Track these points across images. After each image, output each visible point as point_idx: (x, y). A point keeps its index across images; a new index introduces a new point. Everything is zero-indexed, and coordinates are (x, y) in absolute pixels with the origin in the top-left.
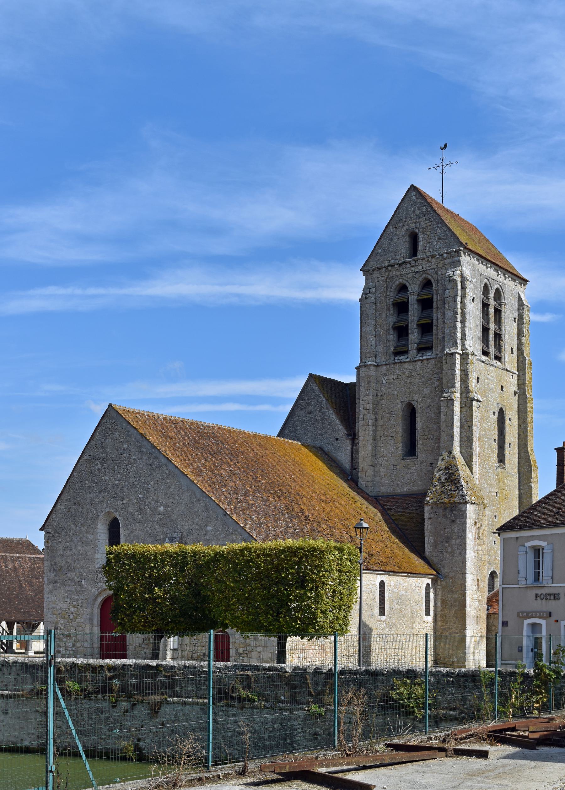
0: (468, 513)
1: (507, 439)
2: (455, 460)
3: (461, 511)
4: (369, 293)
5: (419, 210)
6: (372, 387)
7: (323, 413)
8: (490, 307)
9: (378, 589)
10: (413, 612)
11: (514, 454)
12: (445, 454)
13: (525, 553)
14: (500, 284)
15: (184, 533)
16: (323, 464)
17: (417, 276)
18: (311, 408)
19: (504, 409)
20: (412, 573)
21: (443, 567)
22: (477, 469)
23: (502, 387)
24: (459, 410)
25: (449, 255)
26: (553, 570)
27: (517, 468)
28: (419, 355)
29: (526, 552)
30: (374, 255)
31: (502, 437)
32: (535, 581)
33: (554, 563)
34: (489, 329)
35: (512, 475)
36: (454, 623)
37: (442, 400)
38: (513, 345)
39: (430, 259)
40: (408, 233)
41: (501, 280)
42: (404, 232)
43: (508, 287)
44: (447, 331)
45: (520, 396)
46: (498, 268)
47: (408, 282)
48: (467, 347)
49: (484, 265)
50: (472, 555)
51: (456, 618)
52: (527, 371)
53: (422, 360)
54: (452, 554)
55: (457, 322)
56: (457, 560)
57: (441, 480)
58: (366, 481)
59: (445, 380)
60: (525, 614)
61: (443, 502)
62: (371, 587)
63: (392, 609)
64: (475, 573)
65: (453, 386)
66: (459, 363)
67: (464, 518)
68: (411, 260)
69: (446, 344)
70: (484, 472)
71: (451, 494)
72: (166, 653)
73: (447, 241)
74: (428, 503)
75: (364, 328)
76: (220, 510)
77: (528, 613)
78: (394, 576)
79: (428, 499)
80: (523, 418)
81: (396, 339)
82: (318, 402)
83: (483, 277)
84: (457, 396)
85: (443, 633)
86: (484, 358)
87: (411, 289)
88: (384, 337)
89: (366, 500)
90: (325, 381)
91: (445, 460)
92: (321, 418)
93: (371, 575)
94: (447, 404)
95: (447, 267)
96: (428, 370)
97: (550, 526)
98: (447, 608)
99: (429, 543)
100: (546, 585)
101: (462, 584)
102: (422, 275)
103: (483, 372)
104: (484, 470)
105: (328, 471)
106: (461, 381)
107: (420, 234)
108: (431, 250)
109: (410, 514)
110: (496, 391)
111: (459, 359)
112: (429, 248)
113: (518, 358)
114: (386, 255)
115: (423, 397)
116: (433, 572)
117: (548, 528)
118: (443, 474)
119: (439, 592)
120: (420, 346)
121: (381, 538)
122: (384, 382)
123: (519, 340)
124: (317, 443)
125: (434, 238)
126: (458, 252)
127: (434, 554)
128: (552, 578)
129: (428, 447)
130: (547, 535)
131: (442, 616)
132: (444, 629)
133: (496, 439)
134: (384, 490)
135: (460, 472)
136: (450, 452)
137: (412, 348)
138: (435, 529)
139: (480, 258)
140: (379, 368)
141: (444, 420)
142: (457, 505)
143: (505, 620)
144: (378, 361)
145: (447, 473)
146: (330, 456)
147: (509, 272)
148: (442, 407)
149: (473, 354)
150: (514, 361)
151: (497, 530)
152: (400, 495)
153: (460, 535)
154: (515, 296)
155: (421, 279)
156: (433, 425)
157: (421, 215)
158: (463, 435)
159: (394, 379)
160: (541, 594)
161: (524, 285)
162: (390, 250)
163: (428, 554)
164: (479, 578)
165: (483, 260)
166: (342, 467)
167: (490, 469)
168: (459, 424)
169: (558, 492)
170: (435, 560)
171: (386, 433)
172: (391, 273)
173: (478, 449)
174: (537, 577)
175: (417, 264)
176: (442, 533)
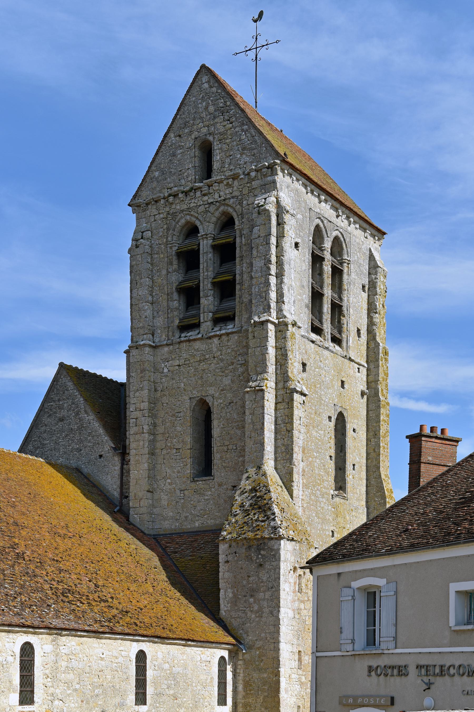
0: (282, 553)
2: (266, 478)
3: (272, 550)
4: (142, 238)
5: (214, 105)
6: (147, 378)
8: (324, 263)
10: (197, 700)
11: (361, 479)
12: (252, 471)
13: (350, 598)
14: (341, 230)
16: (76, 489)
17: (212, 209)
18: (64, 413)
19: (345, 414)
20: (193, 641)
21: (247, 633)
22: (301, 493)
23: (343, 382)
25: (259, 173)
26: (396, 625)
27: (365, 500)
28: (216, 329)
29: (353, 596)
30: (148, 180)
32: (368, 644)
33: (398, 613)
34: (322, 295)
35: (356, 509)
37: (248, 392)
38: (361, 324)
39: (230, 181)
40: (198, 143)
41: (342, 225)
42: (192, 142)
44: (255, 290)
45: (370, 399)
46: (338, 205)
47: (199, 220)
48: (285, 313)
49: (315, 196)
50: (290, 615)
52: (380, 362)
53: (220, 336)
54: (260, 613)
55: (270, 275)
56: (266, 622)
57: (243, 506)
60: (351, 701)
61: (245, 538)
62: (121, 659)
63: (159, 694)
64: (295, 642)
65: (265, 371)
66: (274, 337)
67: (276, 560)
68: (202, 184)
69: (254, 308)
70: (313, 501)
71: (258, 525)
73: (255, 151)
74: (224, 539)
75: (135, 291)
77: (355, 698)
78: (163, 644)
81: (182, 307)
82: (73, 403)
83: (313, 214)
86: (314, 336)
87: (203, 229)
88: (165, 304)
89: (139, 539)
90: (85, 376)
91: (251, 479)
92: (78, 427)
93: (120, 641)
94: (254, 397)
95: (256, 192)
96: (229, 351)
97: (390, 552)
99: (226, 598)
100: (386, 652)
101: (273, 658)
102: (219, 207)
103: (313, 356)
104: (313, 497)
105: (82, 498)
106: (276, 365)
107: (215, 143)
108: (232, 167)
109: (202, 558)
110: (333, 386)
112: (230, 164)
113: (368, 344)
114: (166, 179)
115: (222, 390)
117: (389, 554)
118: (247, 498)
119: (240, 671)
120: (217, 316)
121: (151, 590)
122: (166, 370)
123: (370, 318)
124: (73, 463)
125: (236, 148)
126: (271, 167)
127: (233, 614)
128: (395, 638)
130: (387, 567)
133: (333, 455)
134: (167, 526)
135: (273, 495)
136: (259, 468)
138: (235, 577)
139: (308, 183)
140: (158, 350)
141: (250, 421)
142: (266, 541)
144: (157, 340)
145: (253, 497)
146: (91, 479)
147: (356, 214)
148: (247, 402)
149: (294, 324)
150: (362, 347)
151: (307, 563)
152: (189, 532)
153: (270, 585)
155: (217, 214)
156: (237, 431)
157: (217, 113)
158: (279, 444)
159: (179, 366)
160: (377, 667)
161: (379, 240)
162: (171, 172)
163: (224, 614)
164: (300, 650)
165: (313, 187)
166: (108, 494)
167: (322, 498)
168: (273, 427)
169: (409, 501)
170: (235, 623)
171: (169, 444)
172: (173, 206)
173: (302, 464)
175: (211, 191)
176: (245, 582)
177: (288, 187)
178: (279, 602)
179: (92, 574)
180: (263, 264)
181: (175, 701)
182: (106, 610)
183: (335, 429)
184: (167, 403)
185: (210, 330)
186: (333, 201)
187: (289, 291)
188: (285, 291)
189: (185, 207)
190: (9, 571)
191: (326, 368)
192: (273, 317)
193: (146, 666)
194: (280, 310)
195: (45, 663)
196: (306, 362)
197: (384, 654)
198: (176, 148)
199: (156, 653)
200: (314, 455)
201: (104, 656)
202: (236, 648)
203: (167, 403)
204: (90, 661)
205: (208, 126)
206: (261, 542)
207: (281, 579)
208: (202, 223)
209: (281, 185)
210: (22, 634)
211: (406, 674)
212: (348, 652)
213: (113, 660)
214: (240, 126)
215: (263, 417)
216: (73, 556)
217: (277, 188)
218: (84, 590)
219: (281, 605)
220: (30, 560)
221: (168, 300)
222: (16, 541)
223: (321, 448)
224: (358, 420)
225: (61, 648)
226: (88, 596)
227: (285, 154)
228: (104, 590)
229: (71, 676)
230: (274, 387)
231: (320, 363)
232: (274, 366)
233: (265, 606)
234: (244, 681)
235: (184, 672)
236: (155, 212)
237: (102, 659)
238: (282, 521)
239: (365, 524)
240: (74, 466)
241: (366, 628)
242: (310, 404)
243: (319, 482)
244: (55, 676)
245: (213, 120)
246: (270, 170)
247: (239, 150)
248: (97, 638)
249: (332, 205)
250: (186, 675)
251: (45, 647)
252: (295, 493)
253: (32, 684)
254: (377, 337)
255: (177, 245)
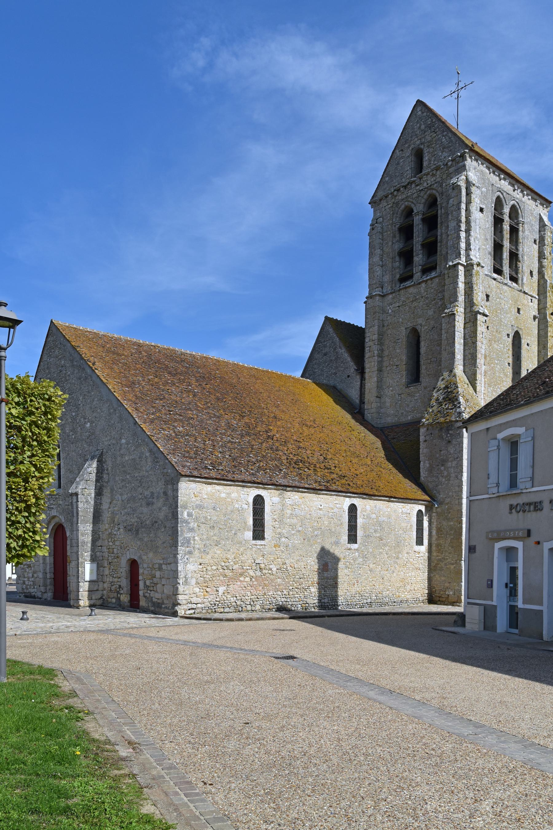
1: (524, 364)
2: (456, 378)
4: (376, 223)
7: (337, 353)
8: (504, 223)
9: (347, 514)
10: (399, 541)
15: (104, 450)
16: (330, 398)
17: (422, 194)
18: (327, 350)
19: (521, 333)
20: (395, 498)
21: (439, 492)
22: (483, 389)
24: (462, 326)
25: (454, 162)
26: (533, 467)
28: (424, 277)
31: (518, 362)
33: (535, 456)
36: (450, 553)
37: (443, 317)
41: (518, 196)
42: (410, 152)
43: (526, 207)
44: (450, 243)
45: (541, 321)
46: (514, 182)
47: (414, 203)
48: (471, 257)
49: (496, 175)
51: (452, 547)
52: (548, 294)
54: (448, 478)
55: (461, 231)
57: (438, 400)
58: (372, 412)
59: (447, 294)
62: (336, 510)
63: (368, 536)
65: (456, 300)
66: (463, 275)
69: (449, 257)
71: (448, 412)
72: (79, 585)
73: (451, 148)
74: (424, 424)
76: (131, 419)
77: (499, 532)
78: (370, 500)
79: (424, 420)
80: (543, 343)
82: (332, 342)
84: (460, 310)
85: (438, 564)
86: (495, 276)
88: (390, 265)
91: (445, 380)
93: (335, 497)
94: (448, 320)
96: (432, 291)
97: (529, 403)
98: (442, 537)
101: (458, 510)
102: (427, 191)
103: (494, 290)
106: (465, 295)
107: (425, 149)
109: (411, 441)
110: (511, 312)
111: (463, 271)
112: (434, 161)
113: (538, 282)
114: (393, 181)
115: (427, 320)
116: (427, 498)
119: (434, 520)
121: (369, 463)
122: (390, 311)
123: (540, 263)
124: (332, 383)
126: (463, 157)
127: (429, 479)
128: (532, 479)
129: (431, 371)
131: (438, 545)
132: (440, 560)
133: (511, 363)
134: (389, 421)
136: (451, 371)
137: (417, 270)
140: (385, 298)
141: (445, 338)
142: (453, 423)
143: (473, 543)
145: (445, 392)
148: (443, 325)
149: (479, 265)
152: (404, 424)
153: (456, 456)
154: (536, 217)
155: (425, 197)
159: (399, 306)
160: (517, 505)
161: (547, 207)
163: (423, 479)
165: (494, 169)
168: (462, 341)
170: (431, 486)
171: (391, 363)
172: (397, 198)
174: (513, 483)
175: (422, 182)
176: (438, 455)
177: (475, 169)
178: (463, 469)
179: (324, 451)
180: (456, 224)
181: (381, 542)
182: (328, 475)
183: (512, 343)
184: (391, 334)
185: (420, 279)
186: (510, 179)
187: (475, 241)
188: (472, 241)
189: (405, 196)
190: (257, 447)
191: (505, 299)
192: (463, 260)
193: (356, 516)
194: (468, 256)
195: (273, 511)
196: (489, 294)
197: (522, 493)
198: (400, 159)
199: (365, 506)
200: (495, 362)
201: (322, 507)
202: (431, 504)
203: (391, 334)
204: (310, 511)
205: (420, 139)
206: (449, 424)
207: (464, 451)
208: (415, 205)
209: (469, 167)
210: (255, 489)
211: (541, 509)
212: (494, 494)
213: (329, 511)
214: (442, 133)
215: (455, 333)
216: (313, 439)
217: (466, 169)
218: (314, 461)
219: (464, 471)
220: (277, 440)
221: (392, 262)
222: (271, 428)
223: (501, 357)
224: (531, 337)
225: (287, 500)
226: (315, 465)
227: (472, 145)
228: (330, 461)
229: (295, 521)
230: (463, 312)
231: (500, 295)
232: (463, 297)
233: (452, 472)
234: (436, 528)
235: (389, 520)
236: (385, 204)
237: (320, 509)
238: (465, 408)
239: (512, 386)
240: (332, 384)
241: (510, 473)
242: (492, 325)
243: (499, 382)
244: (282, 521)
245: (424, 134)
246: (461, 158)
247: (440, 150)
248: (316, 494)
249: (509, 182)
250: (390, 523)
251: (274, 499)
252: (478, 389)
253: (263, 526)
254: (545, 276)
255: (399, 223)
